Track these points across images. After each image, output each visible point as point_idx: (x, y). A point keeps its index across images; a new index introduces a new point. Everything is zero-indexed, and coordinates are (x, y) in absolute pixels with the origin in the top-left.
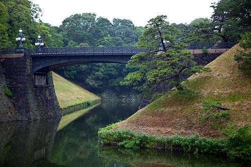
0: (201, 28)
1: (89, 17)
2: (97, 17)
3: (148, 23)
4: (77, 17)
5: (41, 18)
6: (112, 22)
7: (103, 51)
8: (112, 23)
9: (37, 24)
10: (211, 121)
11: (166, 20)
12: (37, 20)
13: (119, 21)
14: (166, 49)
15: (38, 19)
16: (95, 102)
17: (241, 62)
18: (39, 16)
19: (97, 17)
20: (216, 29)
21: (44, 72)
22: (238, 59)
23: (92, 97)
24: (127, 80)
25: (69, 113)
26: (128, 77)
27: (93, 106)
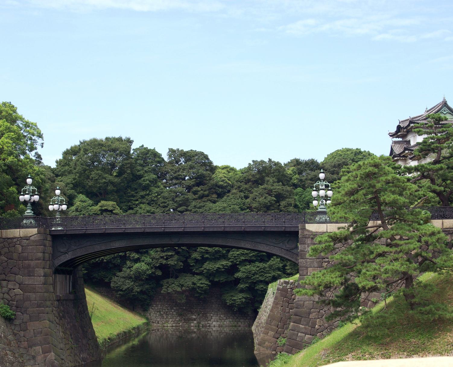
5: (40, 150)
13: (183, 154)
15: (33, 153)
19: (134, 146)
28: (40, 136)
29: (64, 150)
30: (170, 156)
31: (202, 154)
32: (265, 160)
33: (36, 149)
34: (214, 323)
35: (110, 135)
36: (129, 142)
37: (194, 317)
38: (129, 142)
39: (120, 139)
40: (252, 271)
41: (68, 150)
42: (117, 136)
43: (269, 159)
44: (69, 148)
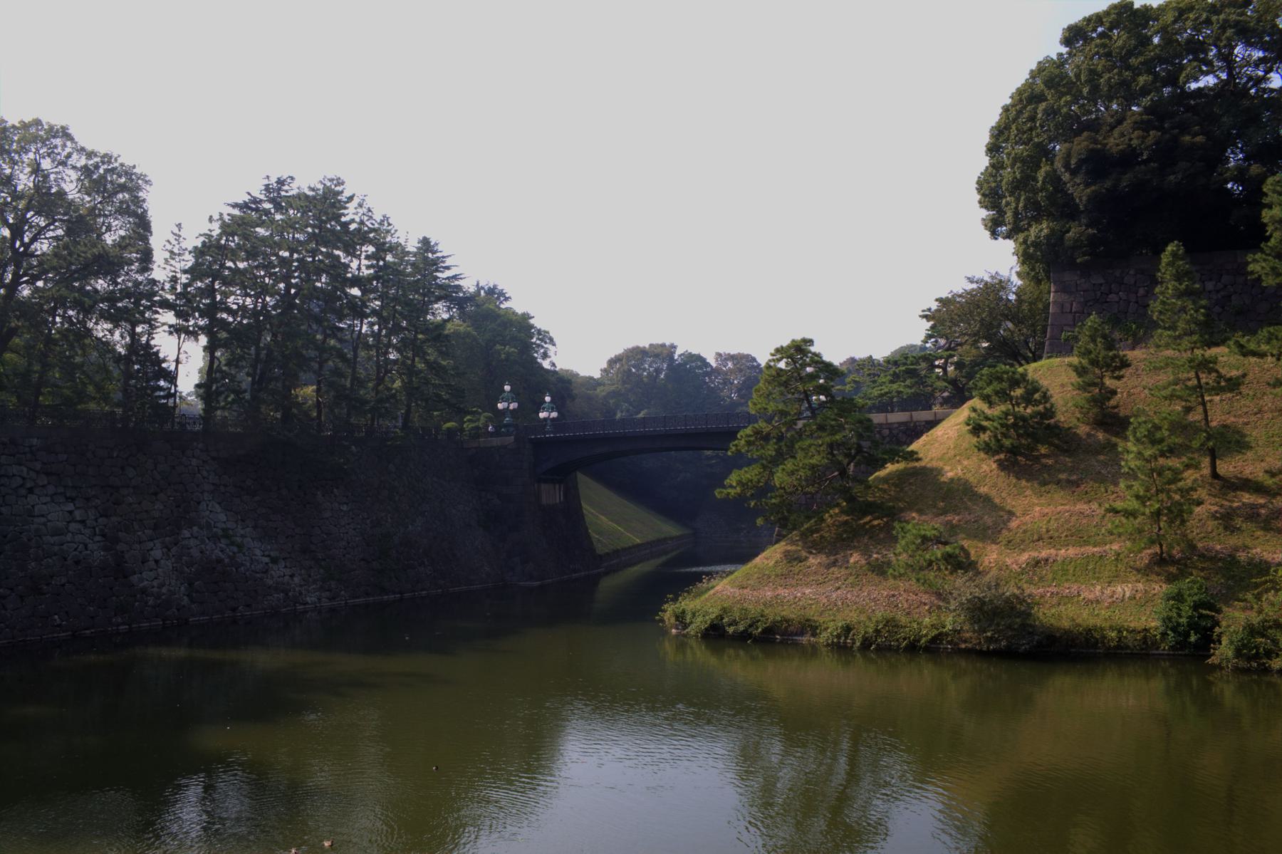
0: (905, 364)
1: (663, 353)
2: (679, 352)
3: (771, 358)
4: (637, 354)
5: (554, 359)
6: (713, 362)
7: (645, 427)
8: (714, 365)
9: (547, 371)
10: (1248, 394)
11: (813, 349)
12: (546, 364)
13: (732, 357)
14: (816, 412)
15: (548, 360)
16: (652, 548)
17: (985, 437)
18: (551, 353)
19: (679, 352)
20: (938, 367)
21: (562, 474)
22: (977, 429)
23: (670, 529)
24: (731, 486)
25: (630, 566)
26: (733, 479)
27: (674, 553)
28: (552, 341)
29: (609, 358)
30: (717, 360)
31: (748, 356)
32: (759, 360)
33: (550, 357)
34: (765, 532)
35: (654, 342)
36: (673, 347)
37: (743, 526)
38: (673, 347)
39: (663, 346)
40: (799, 757)
41: (612, 359)
42: (660, 342)
43: (937, 300)
44: (613, 356)
